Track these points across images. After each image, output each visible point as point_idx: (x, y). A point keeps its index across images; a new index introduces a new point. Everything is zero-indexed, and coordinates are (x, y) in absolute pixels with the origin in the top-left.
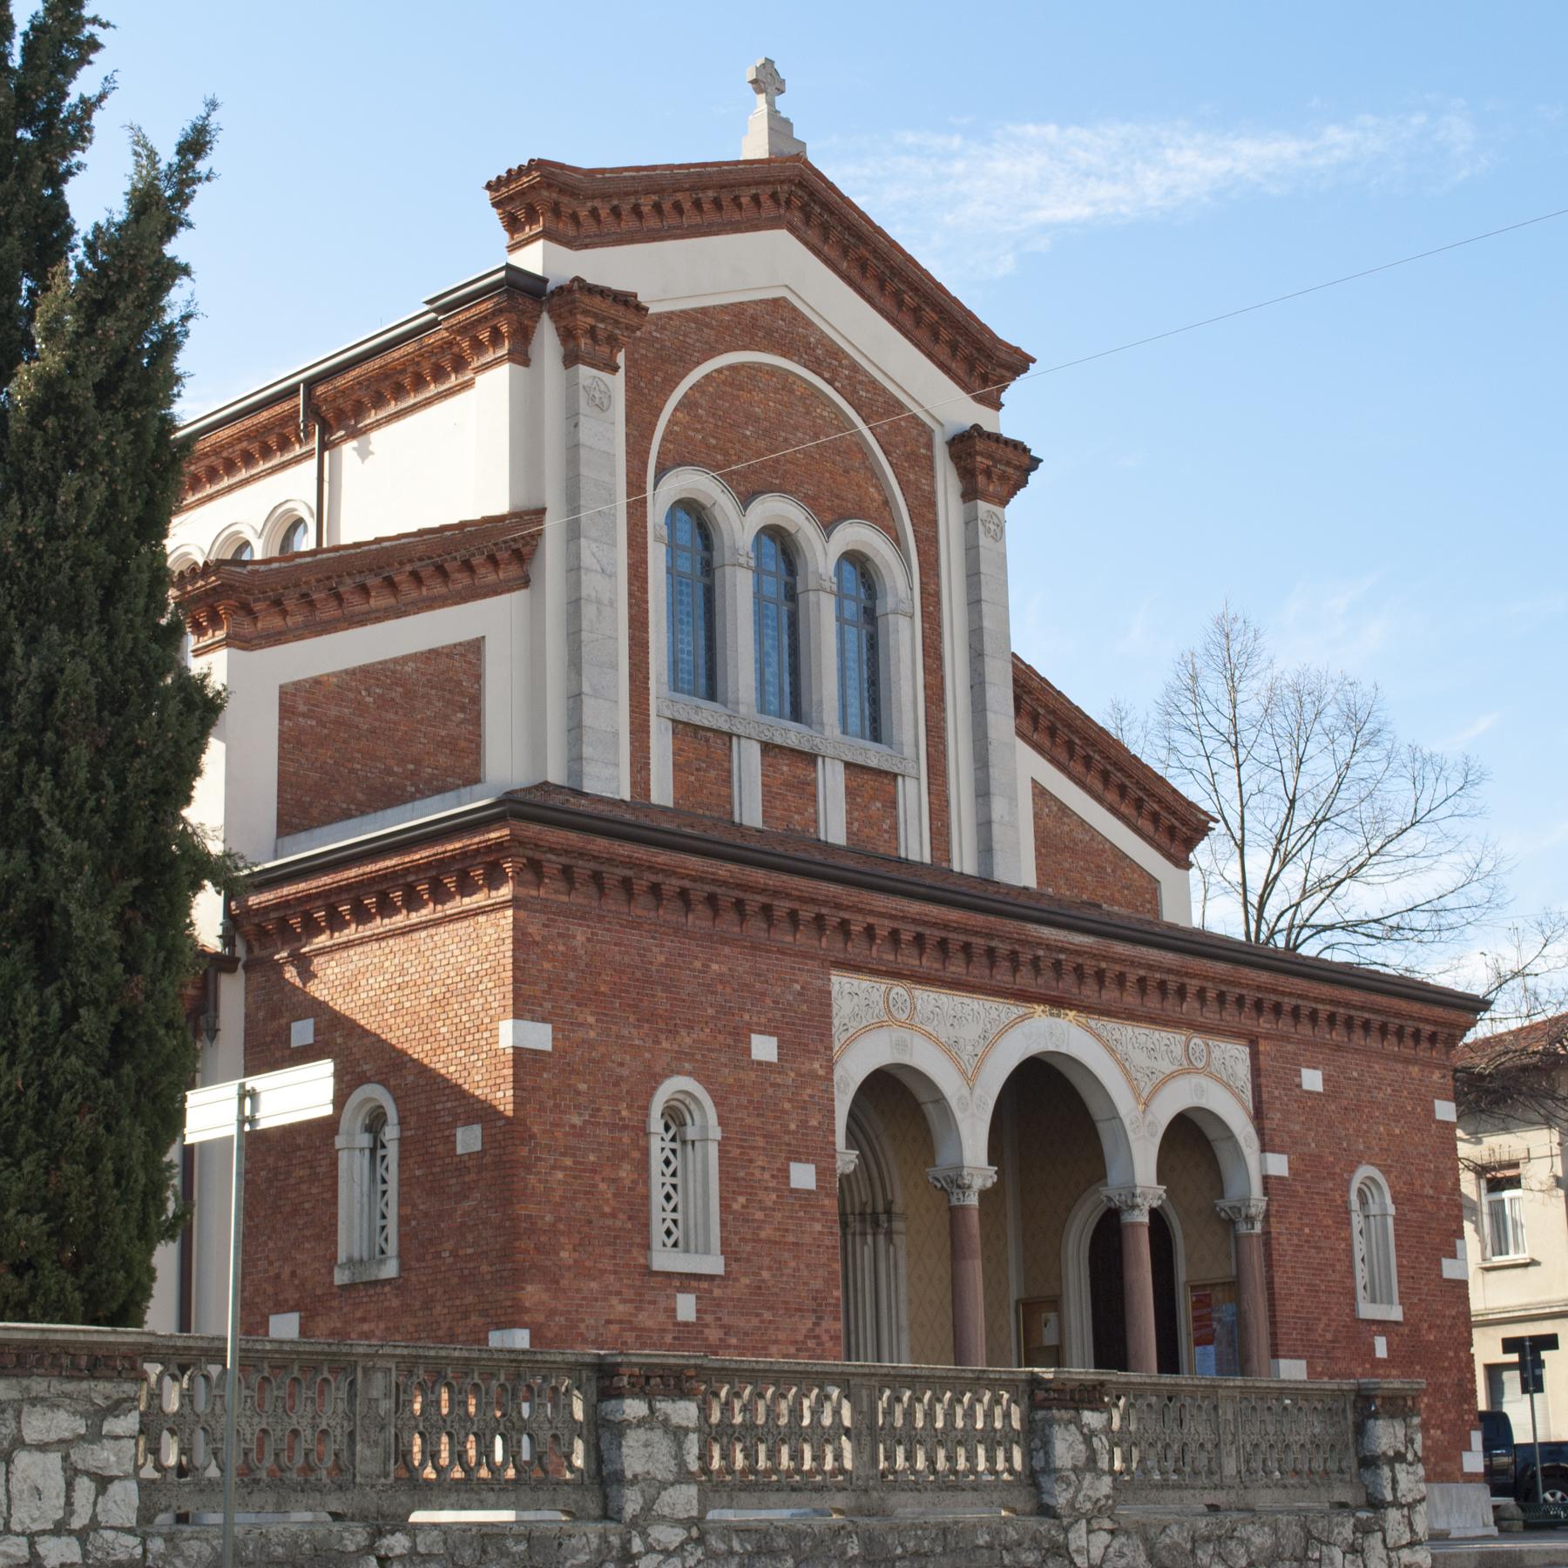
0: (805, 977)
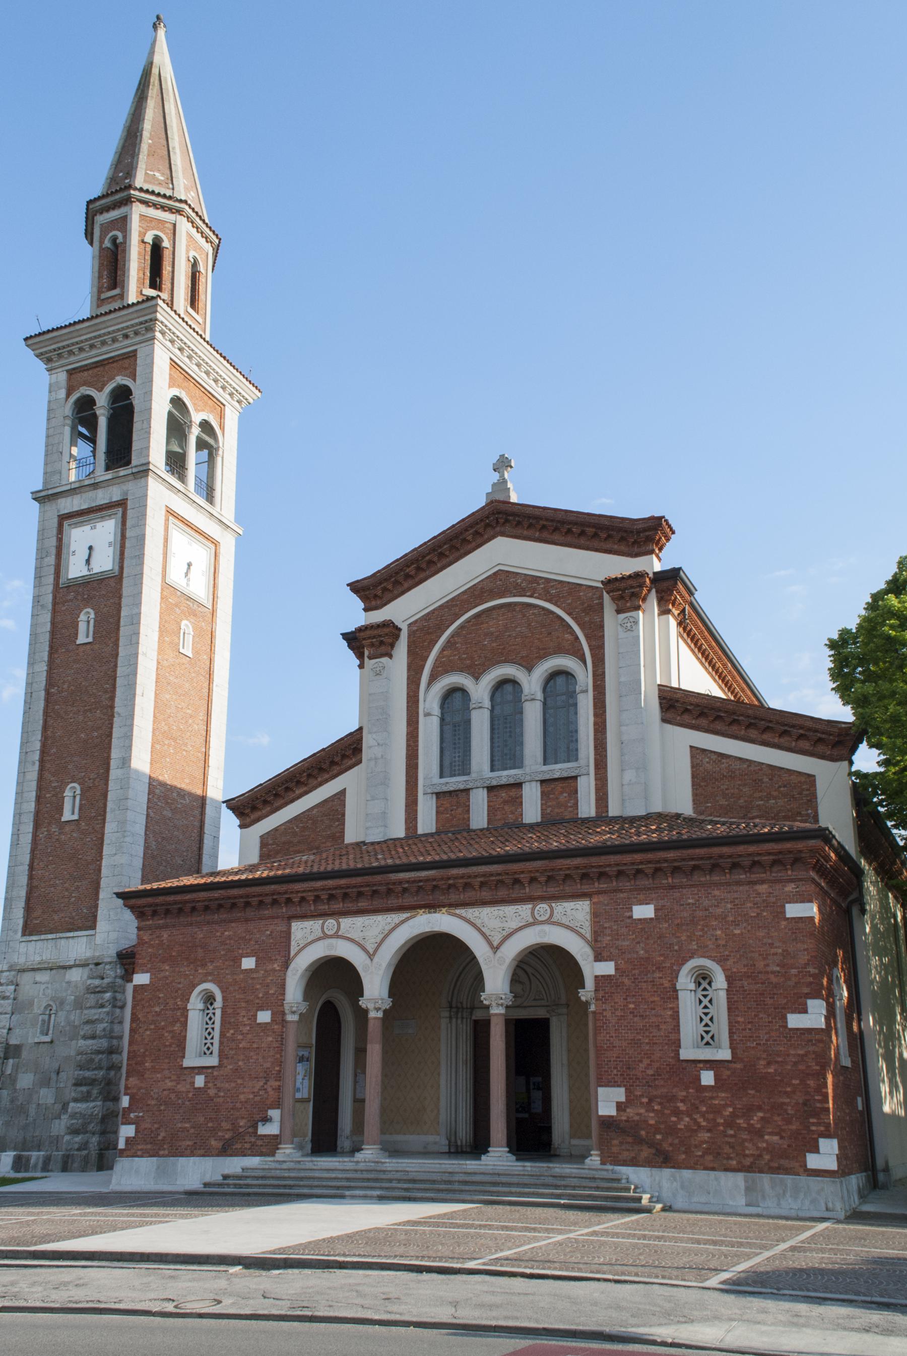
0: (272, 927)
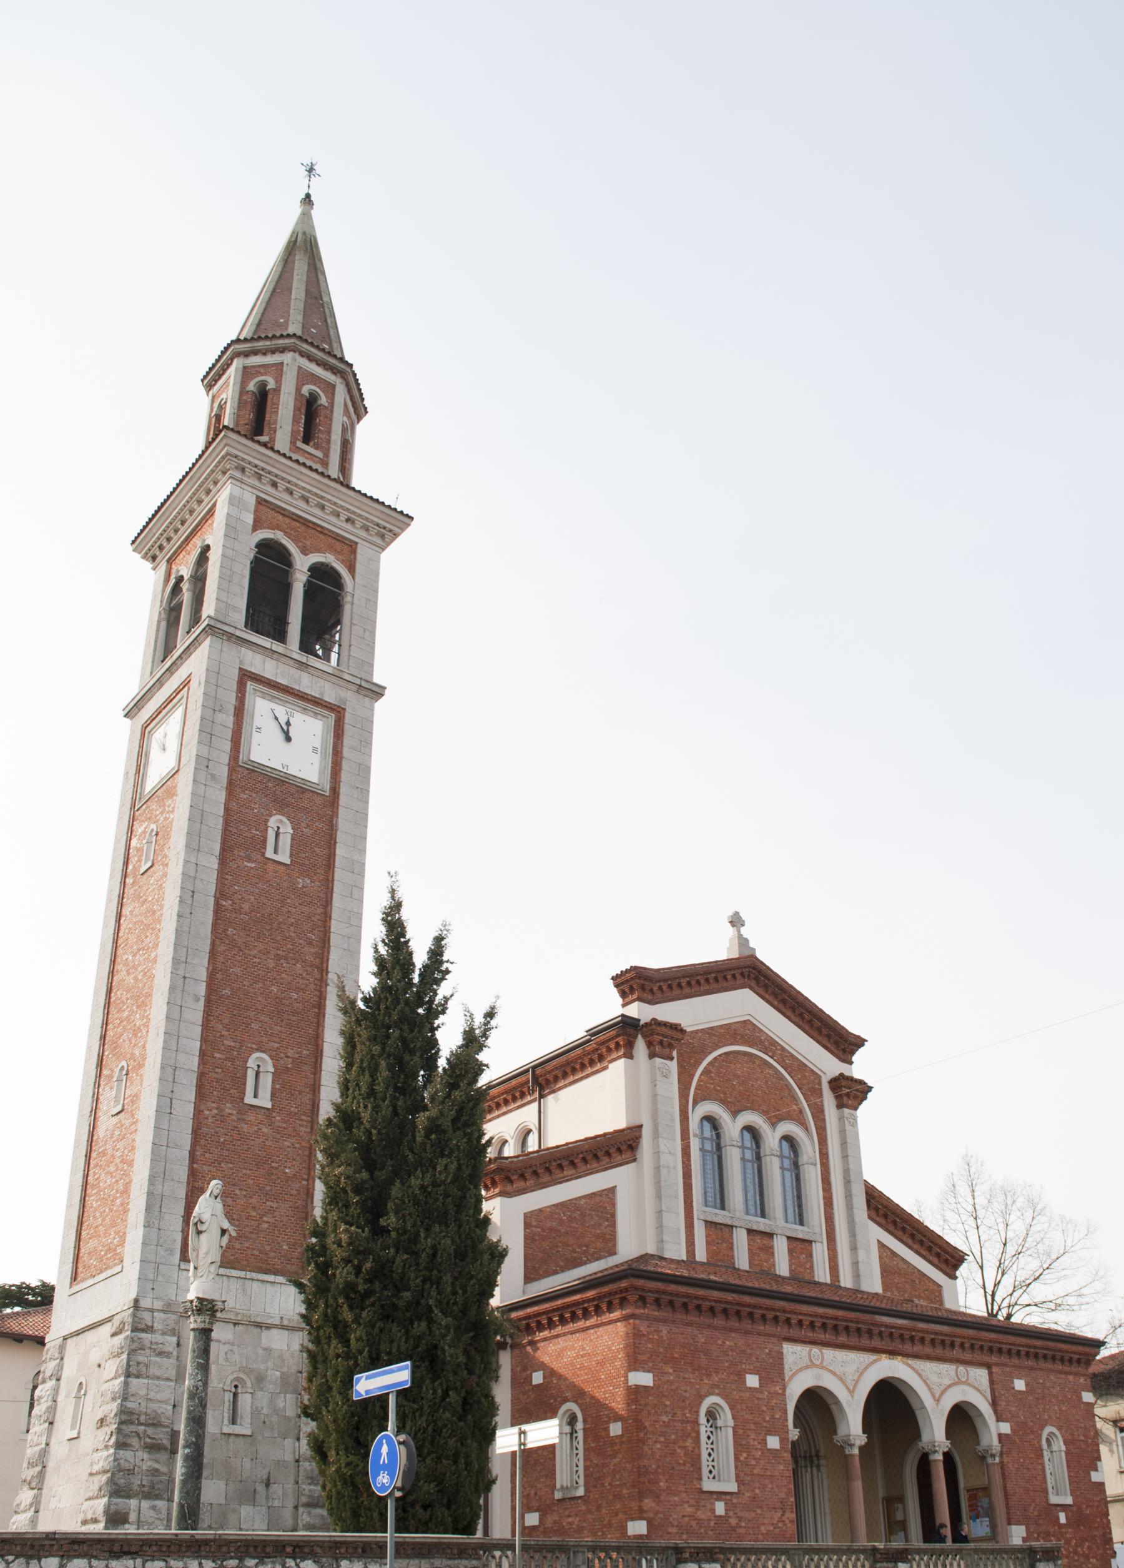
0: (770, 1346)
